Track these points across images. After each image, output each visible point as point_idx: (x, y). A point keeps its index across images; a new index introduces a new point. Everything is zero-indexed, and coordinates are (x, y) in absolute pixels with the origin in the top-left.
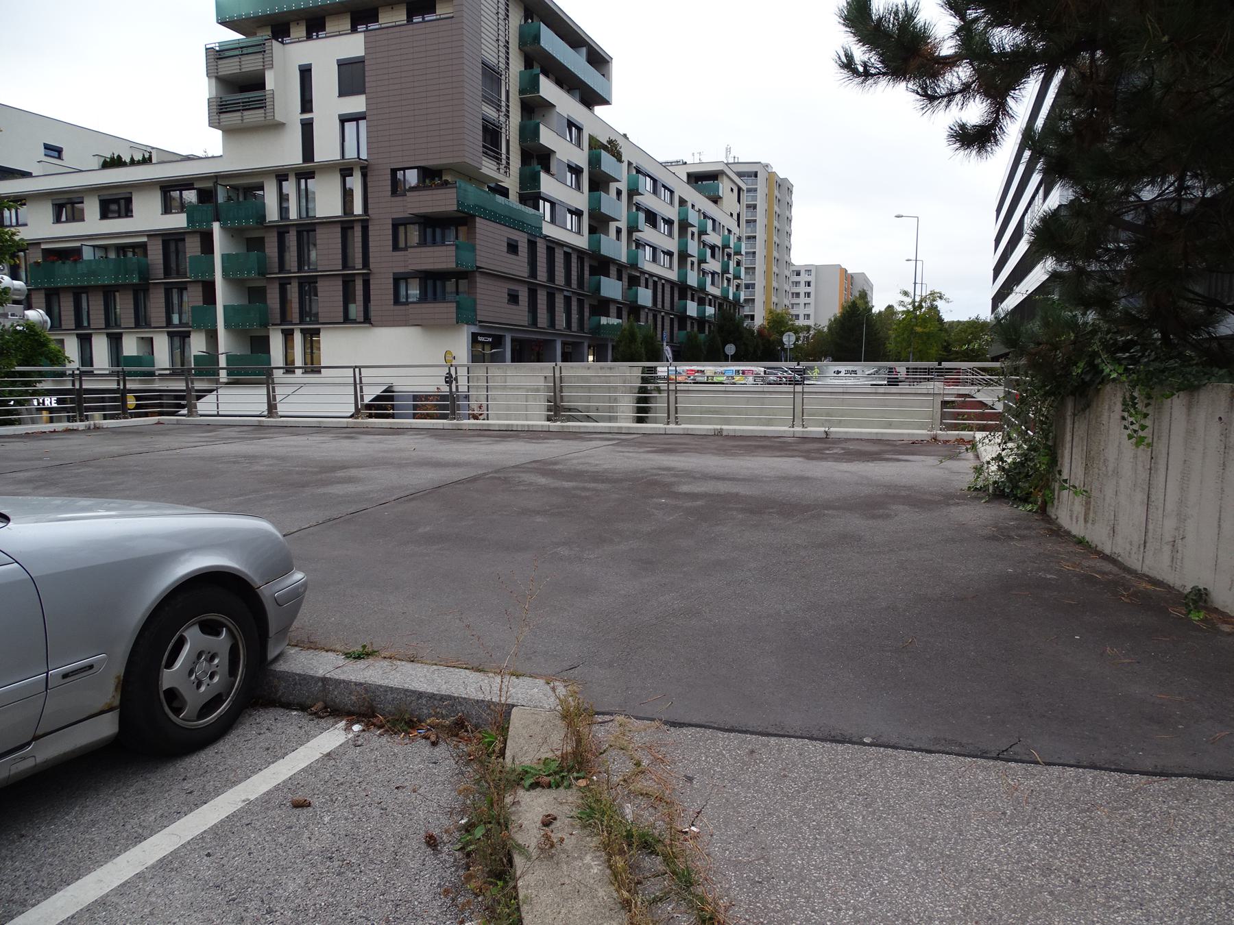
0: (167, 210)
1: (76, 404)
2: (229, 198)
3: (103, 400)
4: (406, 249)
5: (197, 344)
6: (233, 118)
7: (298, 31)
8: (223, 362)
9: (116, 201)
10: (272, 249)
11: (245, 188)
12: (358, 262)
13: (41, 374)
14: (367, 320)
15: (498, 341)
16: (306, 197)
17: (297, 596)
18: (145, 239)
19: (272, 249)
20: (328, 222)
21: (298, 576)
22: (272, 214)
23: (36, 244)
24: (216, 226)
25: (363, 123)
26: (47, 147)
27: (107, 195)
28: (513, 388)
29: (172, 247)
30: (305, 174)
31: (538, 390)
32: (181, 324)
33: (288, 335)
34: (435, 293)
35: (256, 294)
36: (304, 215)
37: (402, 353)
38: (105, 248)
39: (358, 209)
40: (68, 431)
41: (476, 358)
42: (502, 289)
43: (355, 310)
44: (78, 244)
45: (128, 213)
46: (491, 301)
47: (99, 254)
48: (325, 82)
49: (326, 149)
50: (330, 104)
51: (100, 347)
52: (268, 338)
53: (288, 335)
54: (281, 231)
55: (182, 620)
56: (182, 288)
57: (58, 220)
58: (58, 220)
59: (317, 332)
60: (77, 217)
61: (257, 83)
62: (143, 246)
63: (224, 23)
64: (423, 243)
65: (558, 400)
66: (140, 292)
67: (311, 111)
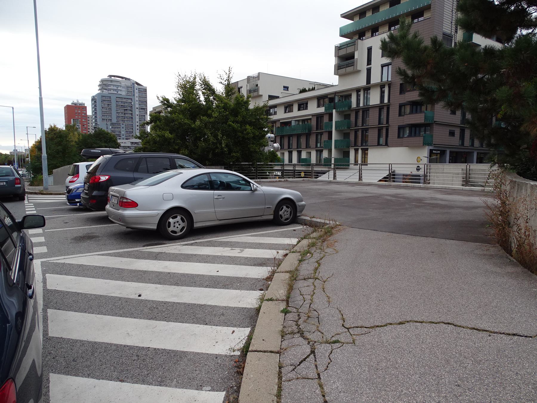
0: (319, 106)
1: (285, 174)
2: (339, 100)
3: (289, 173)
4: (404, 116)
5: (325, 154)
6: (342, 71)
7: (368, 34)
8: (333, 162)
9: (303, 104)
10: (353, 118)
11: (345, 96)
13: (275, 165)
14: (387, 145)
15: (443, 153)
16: (367, 99)
17: (303, 207)
18: (311, 117)
19: (353, 118)
20: (374, 107)
21: (303, 203)
22: (354, 105)
23: (279, 120)
24: (334, 111)
25: (390, 67)
26: (284, 87)
27: (300, 102)
28: (446, 173)
29: (319, 119)
30: (367, 89)
31: (458, 174)
32: (320, 147)
33: (356, 151)
34: (415, 133)
35: (346, 135)
36: (365, 104)
37: (401, 158)
38: (299, 121)
39: (386, 101)
40: (280, 181)
41: (431, 161)
42: (447, 130)
43: (382, 140)
46: (440, 136)
47: (297, 123)
48: (377, 53)
49: (375, 79)
50: (378, 59)
51: (295, 155)
52: (349, 152)
53: (356, 151)
54: (357, 111)
55: (284, 204)
56: (321, 134)
57: (285, 112)
58: (285, 112)
59: (367, 149)
60: (291, 111)
62: (310, 119)
63: (342, 36)
64: (411, 112)
65: (468, 178)
66: (308, 136)
67: (371, 64)
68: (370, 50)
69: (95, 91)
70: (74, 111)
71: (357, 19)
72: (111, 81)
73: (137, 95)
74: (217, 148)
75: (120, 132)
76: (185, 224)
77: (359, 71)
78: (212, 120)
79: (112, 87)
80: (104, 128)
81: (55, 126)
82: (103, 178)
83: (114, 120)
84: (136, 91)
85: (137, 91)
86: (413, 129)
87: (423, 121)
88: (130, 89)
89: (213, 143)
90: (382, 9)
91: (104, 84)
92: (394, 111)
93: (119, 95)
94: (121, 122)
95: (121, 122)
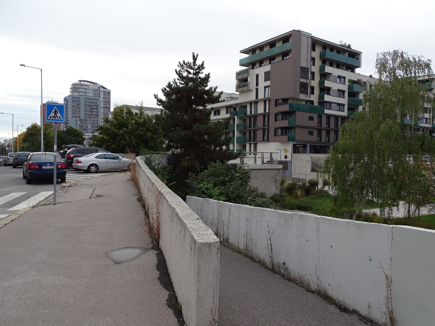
0: (227, 113)
6: (240, 89)
7: (258, 65)
11: (243, 106)
12: (267, 125)
14: (268, 140)
15: (305, 146)
16: (256, 109)
20: (260, 114)
22: (248, 113)
24: (236, 117)
30: (256, 103)
33: (250, 144)
34: (286, 133)
39: (267, 111)
42: (307, 131)
44: (353, 107)
45: (219, 114)
49: (261, 96)
50: (262, 83)
53: (250, 144)
59: (257, 144)
61: (246, 80)
63: (241, 65)
68: (257, 76)
69: (67, 92)
70: (49, 109)
71: (251, 54)
72: (81, 85)
73: (102, 96)
74: (131, 144)
75: (87, 127)
76: (96, 169)
77: (251, 90)
78: (128, 130)
79: (81, 90)
80: (74, 126)
81: (36, 124)
82: (72, 156)
83: (82, 117)
84: (102, 93)
85: (102, 93)
86: (284, 130)
87: (287, 125)
88: (96, 92)
89: (129, 142)
90: (277, 45)
91: (75, 87)
92: (272, 117)
93: (88, 96)
94: (88, 119)
95: (88, 119)
